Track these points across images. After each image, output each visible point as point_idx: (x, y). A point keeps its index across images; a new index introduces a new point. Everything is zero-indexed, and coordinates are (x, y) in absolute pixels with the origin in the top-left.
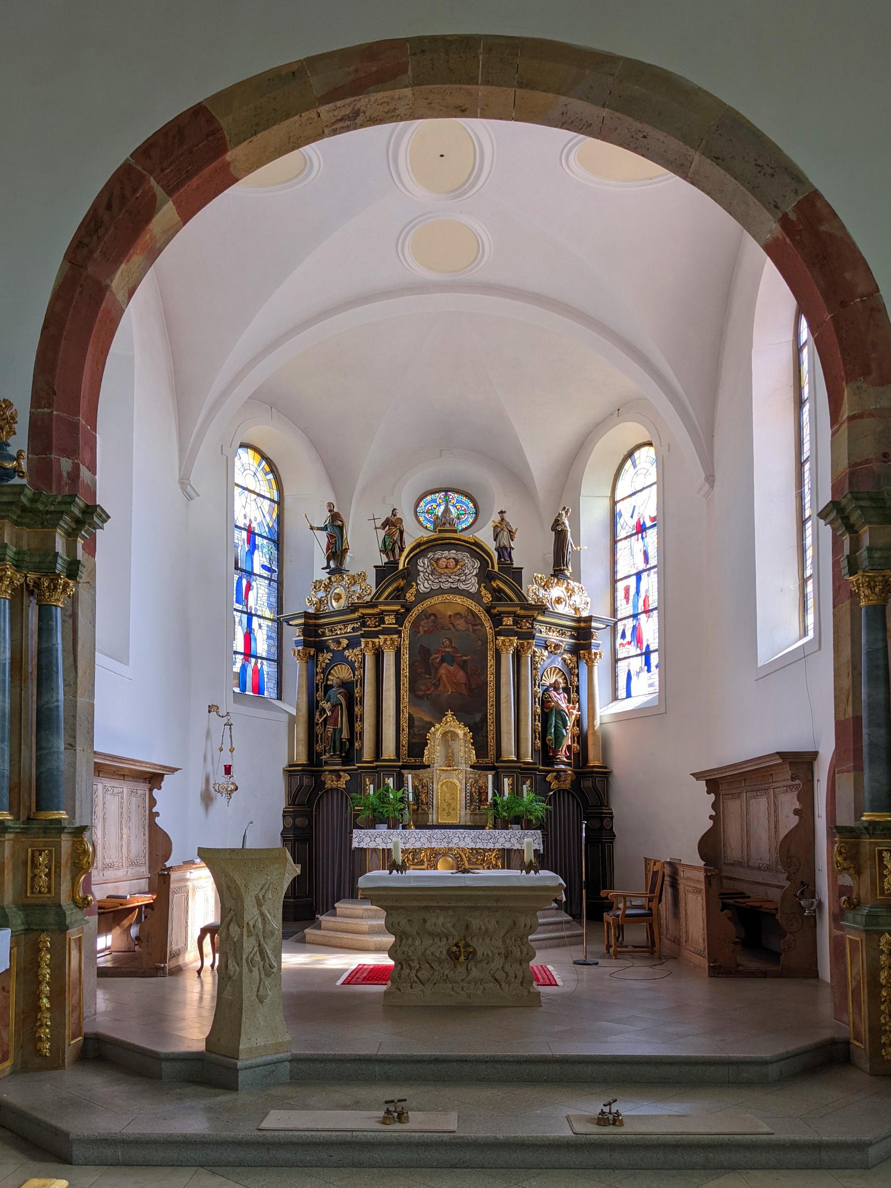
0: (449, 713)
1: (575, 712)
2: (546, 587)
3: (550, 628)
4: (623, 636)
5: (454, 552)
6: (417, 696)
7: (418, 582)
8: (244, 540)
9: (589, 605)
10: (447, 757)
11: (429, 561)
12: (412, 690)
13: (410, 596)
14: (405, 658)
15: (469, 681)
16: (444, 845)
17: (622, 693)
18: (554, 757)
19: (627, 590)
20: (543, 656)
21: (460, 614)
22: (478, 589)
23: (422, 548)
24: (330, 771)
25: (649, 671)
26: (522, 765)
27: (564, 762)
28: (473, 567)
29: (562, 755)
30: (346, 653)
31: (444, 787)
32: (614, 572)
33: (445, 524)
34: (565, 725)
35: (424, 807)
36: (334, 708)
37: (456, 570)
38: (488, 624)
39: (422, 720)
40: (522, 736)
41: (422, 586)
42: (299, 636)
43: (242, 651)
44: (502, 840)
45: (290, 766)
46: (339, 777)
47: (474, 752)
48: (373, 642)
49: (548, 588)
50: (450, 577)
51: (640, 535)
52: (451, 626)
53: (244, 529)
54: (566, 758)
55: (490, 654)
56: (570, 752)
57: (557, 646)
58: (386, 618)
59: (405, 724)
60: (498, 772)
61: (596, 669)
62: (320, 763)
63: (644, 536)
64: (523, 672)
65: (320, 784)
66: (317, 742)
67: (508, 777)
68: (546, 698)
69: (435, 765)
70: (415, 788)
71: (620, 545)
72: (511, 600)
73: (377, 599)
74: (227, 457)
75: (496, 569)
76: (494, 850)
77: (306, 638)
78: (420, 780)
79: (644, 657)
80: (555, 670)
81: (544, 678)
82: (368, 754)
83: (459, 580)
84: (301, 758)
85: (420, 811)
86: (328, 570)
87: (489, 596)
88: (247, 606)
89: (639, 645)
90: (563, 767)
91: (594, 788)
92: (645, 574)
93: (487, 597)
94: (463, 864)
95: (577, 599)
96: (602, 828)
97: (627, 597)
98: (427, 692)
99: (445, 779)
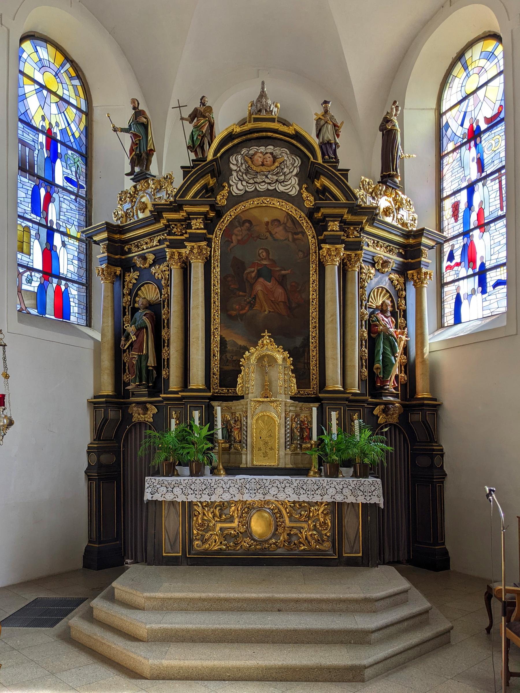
0: (266, 333)
1: (404, 338)
2: (374, 194)
3: (378, 242)
4: (451, 257)
5: (272, 147)
6: (230, 316)
7: (231, 182)
8: (41, 143)
9: (416, 222)
10: (263, 386)
11: (243, 157)
12: (224, 308)
13: (221, 200)
14: (216, 272)
15: (289, 300)
16: (259, 497)
17: (449, 319)
18: (382, 388)
19: (456, 207)
20: (370, 273)
21: (279, 221)
22: (299, 191)
23: (236, 141)
24: (138, 403)
25: (484, 292)
26: (350, 395)
27: (393, 393)
28: (293, 165)
29: (391, 385)
30: (153, 270)
31: (260, 421)
32: (439, 189)
33: (260, 111)
34: (394, 352)
35: (238, 446)
36: (139, 330)
37: (273, 167)
38: (310, 232)
39: (235, 344)
40: (348, 363)
41: (235, 187)
42: (103, 253)
43: (40, 268)
44: (332, 491)
45: (95, 397)
46: (146, 410)
47: (295, 380)
48: (178, 252)
49: (376, 195)
50: (267, 177)
51: (473, 143)
52: (268, 234)
53: (43, 132)
54: (394, 388)
55: (313, 268)
56: (398, 383)
57: (385, 263)
58: (193, 222)
59: (216, 349)
60: (322, 404)
61: (425, 290)
62: (127, 394)
63: (478, 142)
64: (349, 289)
65: (127, 417)
66: (125, 371)
67: (334, 410)
68: (373, 321)
69: (250, 395)
70: (226, 423)
71: (445, 160)
72: (336, 198)
73: (182, 196)
74: (8, 30)
75: (320, 161)
76: (322, 503)
77: (110, 255)
78: (232, 413)
79: (477, 277)
80: (382, 290)
81: (370, 299)
82: (174, 384)
83: (277, 180)
84: (108, 389)
85: (232, 450)
86: (133, 177)
87: (312, 198)
88: (46, 219)
89: (471, 264)
90: (391, 399)
91: (424, 422)
92: (480, 184)
93: (309, 201)
94: (284, 522)
95: (404, 214)
96: (432, 466)
97: (455, 215)
98: (241, 312)
99: (261, 412)
